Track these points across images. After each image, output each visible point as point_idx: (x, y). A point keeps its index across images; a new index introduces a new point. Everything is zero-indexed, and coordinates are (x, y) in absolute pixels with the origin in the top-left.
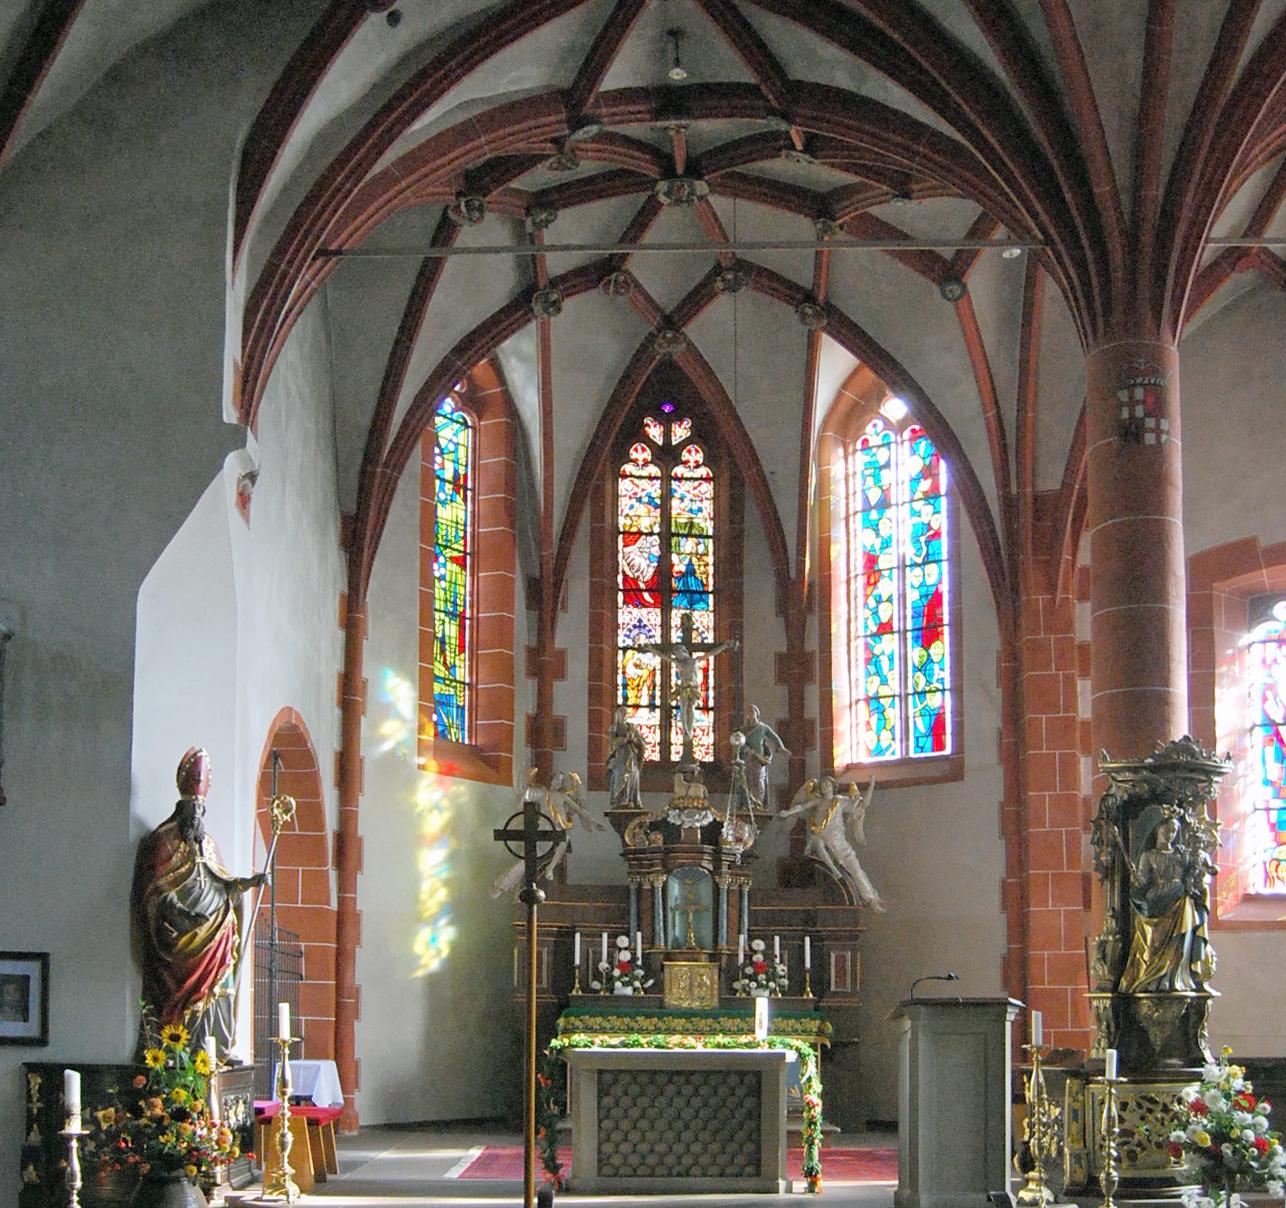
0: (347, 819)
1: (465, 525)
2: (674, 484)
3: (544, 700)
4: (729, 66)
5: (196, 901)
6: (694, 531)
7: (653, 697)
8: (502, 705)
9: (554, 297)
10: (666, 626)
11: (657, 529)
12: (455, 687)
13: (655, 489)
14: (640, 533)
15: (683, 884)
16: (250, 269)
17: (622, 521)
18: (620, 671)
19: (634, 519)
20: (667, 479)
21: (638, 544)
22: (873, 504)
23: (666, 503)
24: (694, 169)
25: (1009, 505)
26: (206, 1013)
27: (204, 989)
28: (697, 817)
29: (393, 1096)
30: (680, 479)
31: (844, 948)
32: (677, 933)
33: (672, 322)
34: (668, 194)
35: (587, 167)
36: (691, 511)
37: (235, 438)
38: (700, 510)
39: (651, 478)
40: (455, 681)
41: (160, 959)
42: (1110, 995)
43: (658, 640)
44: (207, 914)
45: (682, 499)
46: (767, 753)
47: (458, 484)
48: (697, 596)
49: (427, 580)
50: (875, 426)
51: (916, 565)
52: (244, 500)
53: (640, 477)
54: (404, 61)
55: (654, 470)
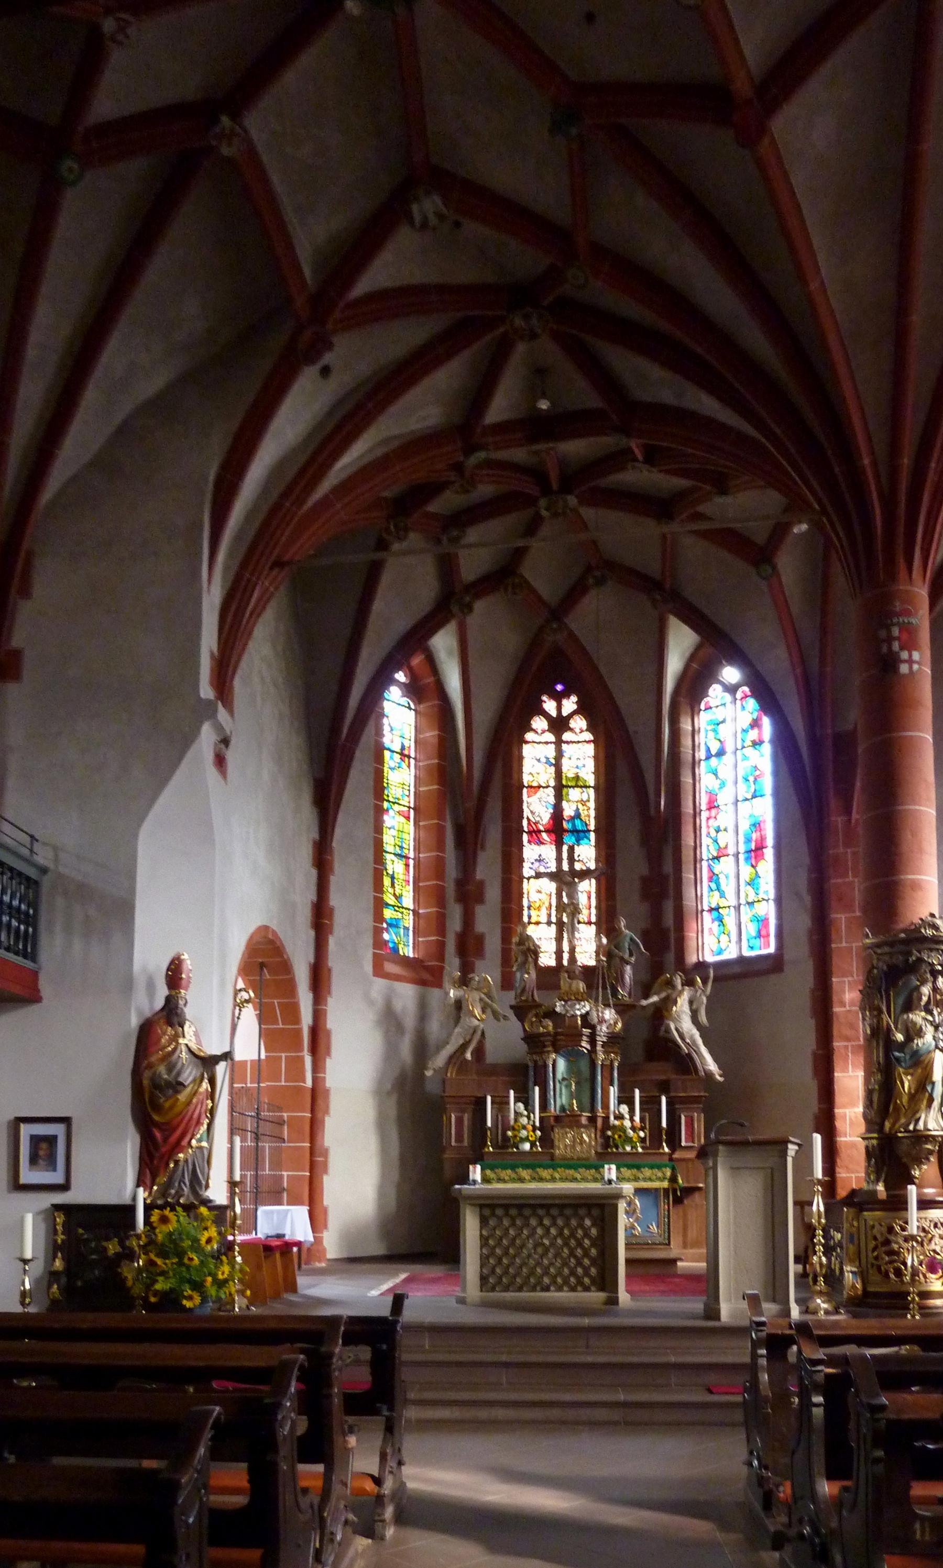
0: (318, 1015)
2: (564, 746)
3: (468, 920)
4: (582, 394)
5: (179, 1074)
6: (581, 783)
7: (549, 915)
9: (467, 599)
10: (559, 859)
12: (402, 913)
13: (551, 751)
15: (568, 1061)
16: (224, 578)
18: (525, 896)
19: (535, 775)
20: (559, 743)
23: (558, 761)
24: (567, 485)
25: (815, 742)
26: (186, 1161)
27: (185, 1143)
28: (578, 1007)
29: (349, 1236)
30: (568, 742)
31: (693, 1110)
33: (558, 612)
34: (547, 509)
35: (485, 490)
36: (577, 767)
37: (206, 711)
39: (547, 743)
40: (403, 908)
41: (152, 1121)
42: (875, 1135)
43: (554, 870)
44: (186, 1084)
46: (631, 955)
47: (403, 755)
48: (582, 834)
49: (378, 828)
51: (747, 799)
52: (220, 761)
54: (340, 403)
55: (551, 737)
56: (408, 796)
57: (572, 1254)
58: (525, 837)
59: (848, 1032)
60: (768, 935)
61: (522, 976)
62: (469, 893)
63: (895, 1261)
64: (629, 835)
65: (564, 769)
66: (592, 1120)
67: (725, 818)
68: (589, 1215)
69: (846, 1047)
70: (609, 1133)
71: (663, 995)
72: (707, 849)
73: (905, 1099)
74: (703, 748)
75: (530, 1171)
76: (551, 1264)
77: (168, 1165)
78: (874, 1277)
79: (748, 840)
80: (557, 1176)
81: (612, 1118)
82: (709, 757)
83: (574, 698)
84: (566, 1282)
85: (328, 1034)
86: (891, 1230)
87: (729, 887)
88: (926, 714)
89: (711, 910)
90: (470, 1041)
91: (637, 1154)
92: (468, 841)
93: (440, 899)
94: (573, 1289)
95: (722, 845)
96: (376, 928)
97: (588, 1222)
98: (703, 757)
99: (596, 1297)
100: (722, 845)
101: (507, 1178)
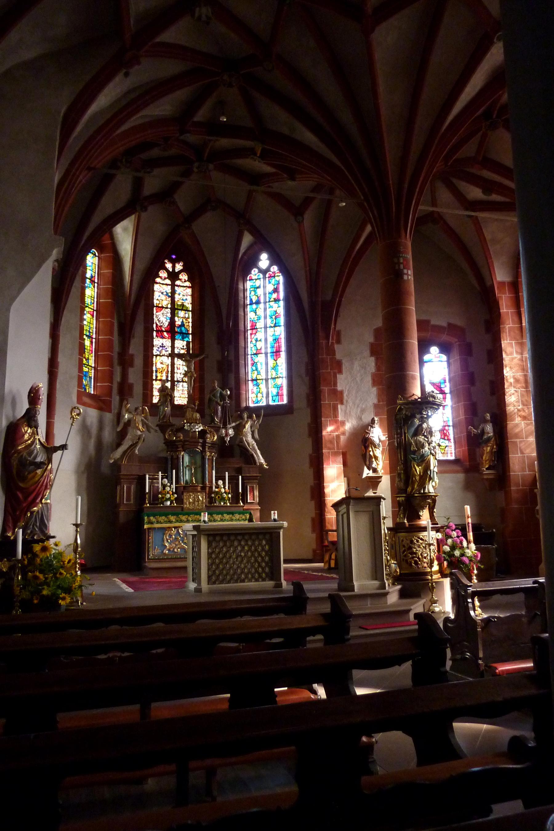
1: (94, 298)
2: (176, 288)
3: (124, 375)
7: (167, 377)
8: (110, 376)
11: (169, 306)
13: (168, 289)
14: (162, 307)
17: (155, 302)
18: (154, 365)
20: (173, 286)
21: (162, 312)
22: (254, 302)
23: (172, 295)
25: (313, 305)
27: (38, 500)
30: (178, 286)
32: (187, 478)
35: (173, 151)
36: (183, 300)
38: (186, 299)
39: (167, 285)
45: (179, 294)
47: (92, 282)
48: (185, 335)
49: (82, 320)
50: (254, 271)
51: (271, 327)
53: (163, 284)
54: (129, 92)
55: (168, 282)
56: (93, 303)
57: (256, 561)
58: (155, 333)
59: (329, 445)
60: (282, 395)
61: (164, 409)
62: (125, 361)
63: (414, 557)
64: (211, 337)
65: (176, 300)
66: (203, 488)
67: (260, 335)
68: (265, 538)
69: (329, 453)
70: (213, 495)
71: (238, 423)
72: (251, 349)
73: (418, 478)
74: (248, 298)
75: (175, 517)
76: (245, 567)
77: (26, 514)
78: (404, 565)
79: (273, 347)
80: (190, 519)
81: (214, 488)
82: (251, 304)
83: (181, 264)
84: (253, 577)
85: (53, 435)
86: (412, 542)
87: (262, 368)
88: (413, 299)
89: (252, 380)
90: (137, 443)
91: (227, 506)
92: (125, 332)
93: (109, 361)
94: (257, 580)
95: (259, 348)
96: (79, 376)
97: (264, 542)
98: (248, 303)
99: (269, 584)
100: (259, 348)
101: (162, 521)
